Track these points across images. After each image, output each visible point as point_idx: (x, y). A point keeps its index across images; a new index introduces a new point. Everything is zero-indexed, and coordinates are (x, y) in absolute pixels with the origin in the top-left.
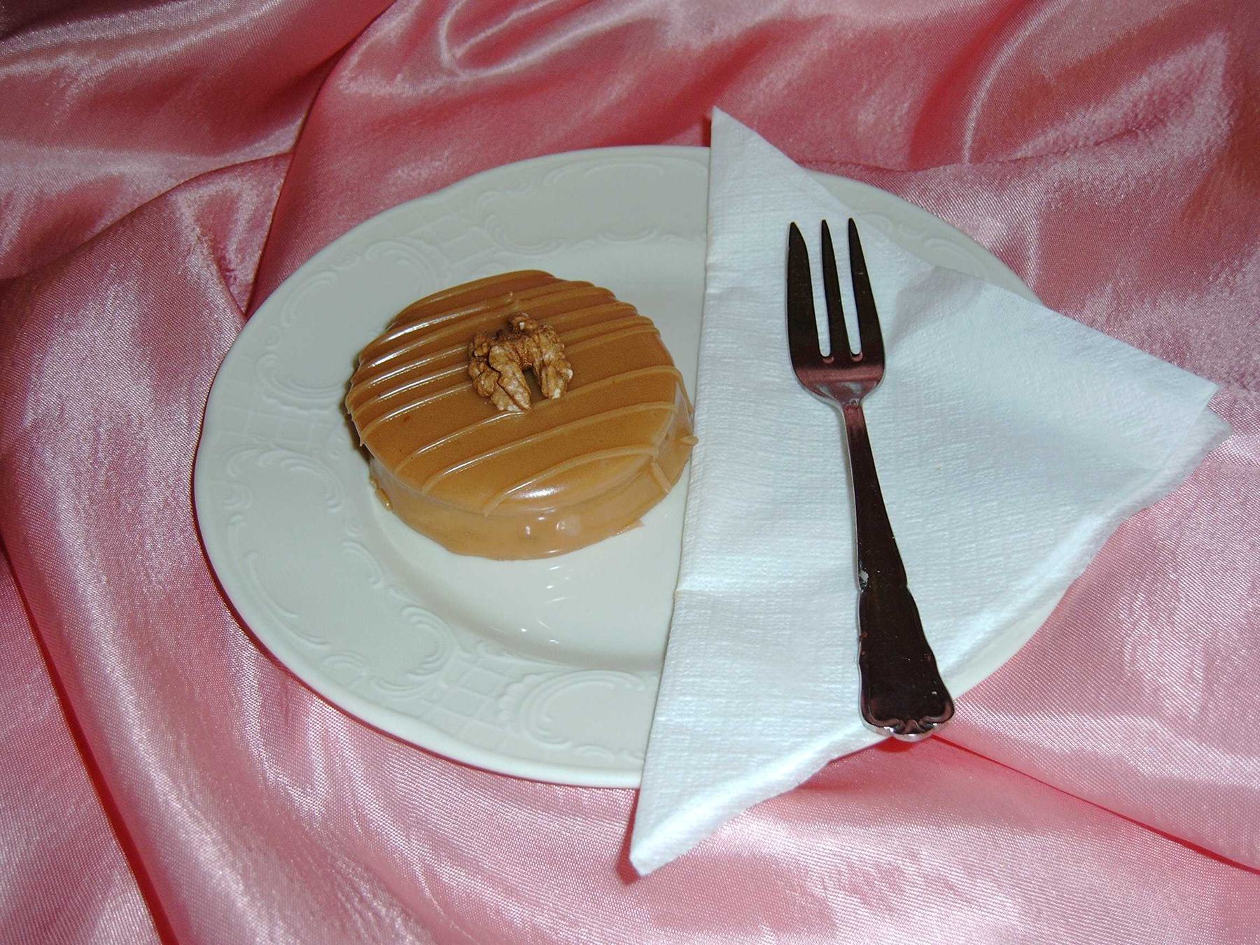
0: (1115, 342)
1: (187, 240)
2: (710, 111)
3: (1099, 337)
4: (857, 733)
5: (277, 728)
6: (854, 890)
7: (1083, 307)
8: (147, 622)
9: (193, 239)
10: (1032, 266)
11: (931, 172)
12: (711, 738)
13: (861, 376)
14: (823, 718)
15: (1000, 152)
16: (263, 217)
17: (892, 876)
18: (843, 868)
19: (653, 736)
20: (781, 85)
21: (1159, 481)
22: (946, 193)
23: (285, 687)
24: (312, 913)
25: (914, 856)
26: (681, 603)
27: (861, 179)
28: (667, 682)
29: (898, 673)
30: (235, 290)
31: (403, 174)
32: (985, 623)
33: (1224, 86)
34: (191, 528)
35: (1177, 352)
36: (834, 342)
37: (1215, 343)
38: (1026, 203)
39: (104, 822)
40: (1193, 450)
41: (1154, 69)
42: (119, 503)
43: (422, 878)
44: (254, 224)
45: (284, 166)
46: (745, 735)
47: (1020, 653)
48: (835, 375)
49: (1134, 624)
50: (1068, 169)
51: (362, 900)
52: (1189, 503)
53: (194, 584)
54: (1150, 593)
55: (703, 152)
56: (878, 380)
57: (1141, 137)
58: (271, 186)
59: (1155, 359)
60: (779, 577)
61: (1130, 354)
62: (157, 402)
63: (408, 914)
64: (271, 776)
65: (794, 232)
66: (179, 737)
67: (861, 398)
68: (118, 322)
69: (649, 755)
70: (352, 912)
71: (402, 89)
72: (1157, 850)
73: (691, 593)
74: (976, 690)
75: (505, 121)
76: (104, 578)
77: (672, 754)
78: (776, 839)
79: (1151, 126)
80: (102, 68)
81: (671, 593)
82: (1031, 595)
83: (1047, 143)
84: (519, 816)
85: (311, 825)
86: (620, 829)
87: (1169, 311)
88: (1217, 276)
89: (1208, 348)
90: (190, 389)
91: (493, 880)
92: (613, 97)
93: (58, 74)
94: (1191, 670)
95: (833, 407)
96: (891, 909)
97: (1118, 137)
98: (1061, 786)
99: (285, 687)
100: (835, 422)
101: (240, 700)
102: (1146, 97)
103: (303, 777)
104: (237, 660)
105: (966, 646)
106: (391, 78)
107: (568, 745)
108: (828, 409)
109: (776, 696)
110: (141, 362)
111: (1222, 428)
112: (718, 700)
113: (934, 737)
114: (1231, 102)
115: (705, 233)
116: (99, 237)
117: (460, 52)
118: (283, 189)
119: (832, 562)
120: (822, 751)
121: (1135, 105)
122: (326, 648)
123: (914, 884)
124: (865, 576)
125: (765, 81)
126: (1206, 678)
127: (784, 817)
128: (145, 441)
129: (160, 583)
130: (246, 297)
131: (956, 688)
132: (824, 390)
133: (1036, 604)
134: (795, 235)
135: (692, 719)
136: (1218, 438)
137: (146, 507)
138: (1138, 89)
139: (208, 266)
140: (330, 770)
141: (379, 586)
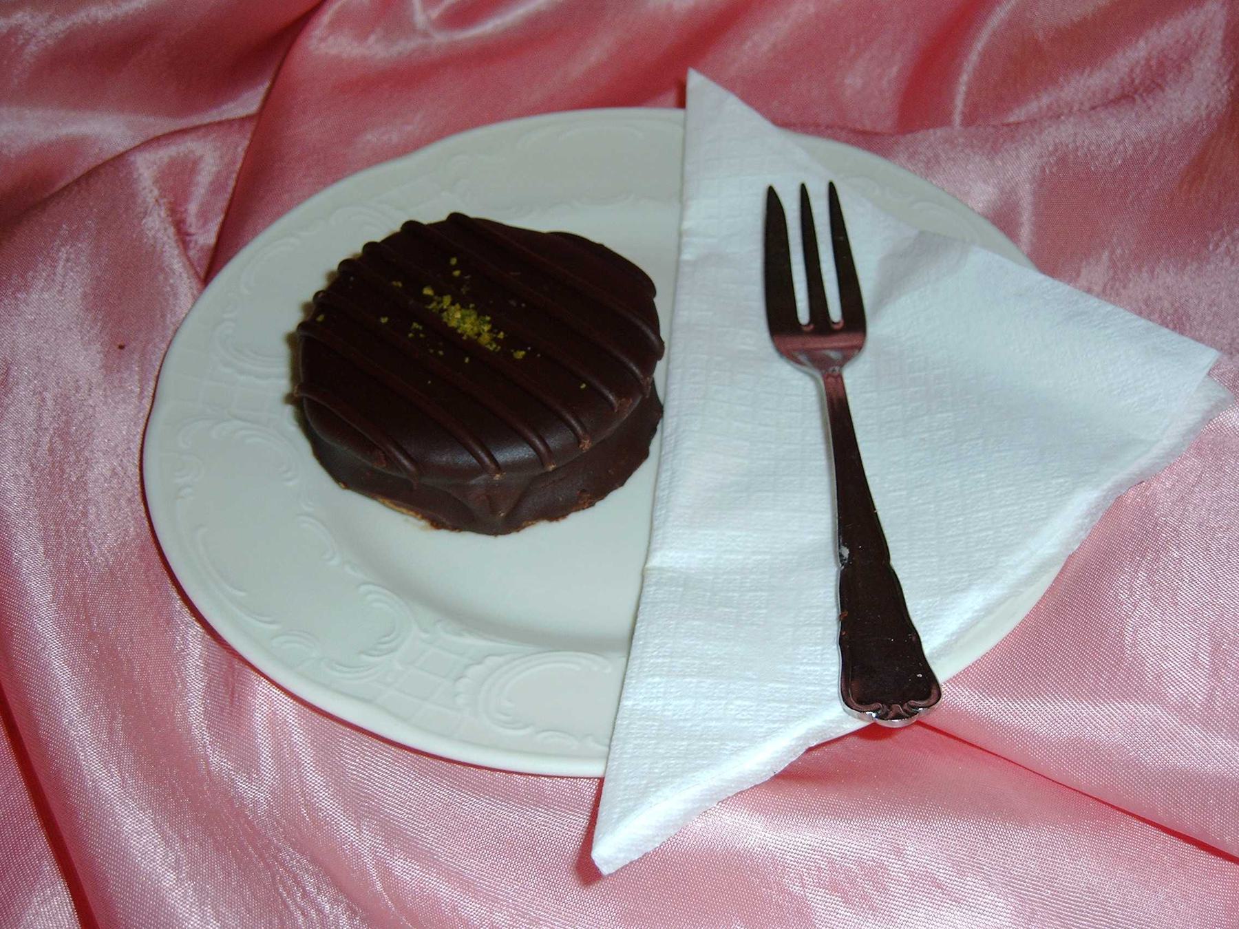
0: (1110, 308)
1: (144, 201)
2: (685, 73)
3: (1094, 302)
4: (837, 718)
5: (222, 709)
6: (834, 887)
7: (1078, 275)
8: (85, 595)
9: (151, 200)
10: (1026, 232)
11: (919, 135)
12: (681, 724)
13: (842, 344)
14: (800, 703)
15: (992, 118)
16: (227, 178)
17: (875, 874)
18: (823, 865)
19: (618, 722)
20: (765, 47)
21: (1157, 451)
22: (937, 156)
23: (231, 667)
24: (249, 911)
25: (899, 852)
26: (651, 580)
27: (847, 142)
28: (635, 664)
29: (881, 653)
30: (192, 253)
31: (371, 138)
32: (973, 602)
33: (1223, 51)
34: (139, 498)
35: (1178, 321)
36: (813, 311)
37: (1216, 314)
38: (1021, 167)
39: (30, 811)
40: (1192, 418)
41: (1152, 34)
42: (63, 471)
43: (373, 872)
44: (216, 187)
45: (250, 127)
46: (718, 720)
47: (1012, 633)
48: (815, 343)
49: (1135, 606)
50: (1064, 133)
51: (305, 894)
52: (1192, 479)
53: (140, 557)
54: (1151, 572)
55: (679, 113)
56: (859, 348)
57: (1139, 100)
58: (236, 148)
59: (1151, 324)
60: (754, 553)
61: (1124, 319)
62: (108, 369)
63: (355, 913)
64: (214, 760)
65: (772, 196)
66: (114, 717)
67: (841, 366)
68: (69, 284)
69: (614, 743)
70: (293, 908)
71: (377, 50)
72: (1158, 846)
73: (661, 569)
74: (966, 671)
75: (484, 81)
76: (41, 549)
77: (639, 741)
78: (755, 832)
79: (1149, 90)
80: (60, 26)
81: (640, 568)
82: (1022, 572)
83: (1040, 108)
84: (476, 807)
85: (255, 813)
86: (583, 821)
87: (1168, 280)
88: (1217, 246)
89: (1208, 319)
90: (143, 355)
91: (451, 875)
92: (593, 59)
93: (14, 31)
94: (1196, 654)
95: (813, 377)
96: (873, 908)
97: (1116, 101)
98: (1055, 777)
99: (231, 667)
100: (814, 393)
101: (183, 681)
102: (1143, 62)
103: (248, 762)
104: (183, 638)
105: (951, 627)
106: (362, 36)
107: (529, 730)
108: (807, 379)
109: (751, 679)
110: (92, 328)
111: (1223, 395)
112: (688, 680)
113: (919, 723)
114: (1231, 68)
115: (681, 199)
116: (52, 196)
117: (435, 13)
118: (248, 151)
119: (811, 537)
120: (799, 738)
121: (1132, 70)
122: (274, 627)
123: (899, 882)
124: (846, 552)
125: (749, 44)
126: (1213, 663)
127: (761, 809)
128: (94, 408)
129: (103, 555)
130: (205, 263)
131: (943, 671)
132: (802, 358)
133: (1029, 580)
134: (772, 197)
135: (661, 702)
136: (1218, 407)
137: (91, 476)
138: (1134, 55)
139: (165, 229)
140: (277, 755)
141: (335, 562)
